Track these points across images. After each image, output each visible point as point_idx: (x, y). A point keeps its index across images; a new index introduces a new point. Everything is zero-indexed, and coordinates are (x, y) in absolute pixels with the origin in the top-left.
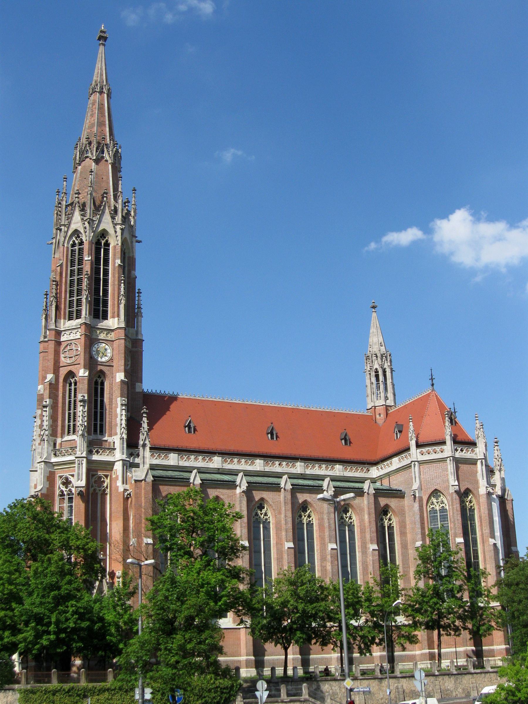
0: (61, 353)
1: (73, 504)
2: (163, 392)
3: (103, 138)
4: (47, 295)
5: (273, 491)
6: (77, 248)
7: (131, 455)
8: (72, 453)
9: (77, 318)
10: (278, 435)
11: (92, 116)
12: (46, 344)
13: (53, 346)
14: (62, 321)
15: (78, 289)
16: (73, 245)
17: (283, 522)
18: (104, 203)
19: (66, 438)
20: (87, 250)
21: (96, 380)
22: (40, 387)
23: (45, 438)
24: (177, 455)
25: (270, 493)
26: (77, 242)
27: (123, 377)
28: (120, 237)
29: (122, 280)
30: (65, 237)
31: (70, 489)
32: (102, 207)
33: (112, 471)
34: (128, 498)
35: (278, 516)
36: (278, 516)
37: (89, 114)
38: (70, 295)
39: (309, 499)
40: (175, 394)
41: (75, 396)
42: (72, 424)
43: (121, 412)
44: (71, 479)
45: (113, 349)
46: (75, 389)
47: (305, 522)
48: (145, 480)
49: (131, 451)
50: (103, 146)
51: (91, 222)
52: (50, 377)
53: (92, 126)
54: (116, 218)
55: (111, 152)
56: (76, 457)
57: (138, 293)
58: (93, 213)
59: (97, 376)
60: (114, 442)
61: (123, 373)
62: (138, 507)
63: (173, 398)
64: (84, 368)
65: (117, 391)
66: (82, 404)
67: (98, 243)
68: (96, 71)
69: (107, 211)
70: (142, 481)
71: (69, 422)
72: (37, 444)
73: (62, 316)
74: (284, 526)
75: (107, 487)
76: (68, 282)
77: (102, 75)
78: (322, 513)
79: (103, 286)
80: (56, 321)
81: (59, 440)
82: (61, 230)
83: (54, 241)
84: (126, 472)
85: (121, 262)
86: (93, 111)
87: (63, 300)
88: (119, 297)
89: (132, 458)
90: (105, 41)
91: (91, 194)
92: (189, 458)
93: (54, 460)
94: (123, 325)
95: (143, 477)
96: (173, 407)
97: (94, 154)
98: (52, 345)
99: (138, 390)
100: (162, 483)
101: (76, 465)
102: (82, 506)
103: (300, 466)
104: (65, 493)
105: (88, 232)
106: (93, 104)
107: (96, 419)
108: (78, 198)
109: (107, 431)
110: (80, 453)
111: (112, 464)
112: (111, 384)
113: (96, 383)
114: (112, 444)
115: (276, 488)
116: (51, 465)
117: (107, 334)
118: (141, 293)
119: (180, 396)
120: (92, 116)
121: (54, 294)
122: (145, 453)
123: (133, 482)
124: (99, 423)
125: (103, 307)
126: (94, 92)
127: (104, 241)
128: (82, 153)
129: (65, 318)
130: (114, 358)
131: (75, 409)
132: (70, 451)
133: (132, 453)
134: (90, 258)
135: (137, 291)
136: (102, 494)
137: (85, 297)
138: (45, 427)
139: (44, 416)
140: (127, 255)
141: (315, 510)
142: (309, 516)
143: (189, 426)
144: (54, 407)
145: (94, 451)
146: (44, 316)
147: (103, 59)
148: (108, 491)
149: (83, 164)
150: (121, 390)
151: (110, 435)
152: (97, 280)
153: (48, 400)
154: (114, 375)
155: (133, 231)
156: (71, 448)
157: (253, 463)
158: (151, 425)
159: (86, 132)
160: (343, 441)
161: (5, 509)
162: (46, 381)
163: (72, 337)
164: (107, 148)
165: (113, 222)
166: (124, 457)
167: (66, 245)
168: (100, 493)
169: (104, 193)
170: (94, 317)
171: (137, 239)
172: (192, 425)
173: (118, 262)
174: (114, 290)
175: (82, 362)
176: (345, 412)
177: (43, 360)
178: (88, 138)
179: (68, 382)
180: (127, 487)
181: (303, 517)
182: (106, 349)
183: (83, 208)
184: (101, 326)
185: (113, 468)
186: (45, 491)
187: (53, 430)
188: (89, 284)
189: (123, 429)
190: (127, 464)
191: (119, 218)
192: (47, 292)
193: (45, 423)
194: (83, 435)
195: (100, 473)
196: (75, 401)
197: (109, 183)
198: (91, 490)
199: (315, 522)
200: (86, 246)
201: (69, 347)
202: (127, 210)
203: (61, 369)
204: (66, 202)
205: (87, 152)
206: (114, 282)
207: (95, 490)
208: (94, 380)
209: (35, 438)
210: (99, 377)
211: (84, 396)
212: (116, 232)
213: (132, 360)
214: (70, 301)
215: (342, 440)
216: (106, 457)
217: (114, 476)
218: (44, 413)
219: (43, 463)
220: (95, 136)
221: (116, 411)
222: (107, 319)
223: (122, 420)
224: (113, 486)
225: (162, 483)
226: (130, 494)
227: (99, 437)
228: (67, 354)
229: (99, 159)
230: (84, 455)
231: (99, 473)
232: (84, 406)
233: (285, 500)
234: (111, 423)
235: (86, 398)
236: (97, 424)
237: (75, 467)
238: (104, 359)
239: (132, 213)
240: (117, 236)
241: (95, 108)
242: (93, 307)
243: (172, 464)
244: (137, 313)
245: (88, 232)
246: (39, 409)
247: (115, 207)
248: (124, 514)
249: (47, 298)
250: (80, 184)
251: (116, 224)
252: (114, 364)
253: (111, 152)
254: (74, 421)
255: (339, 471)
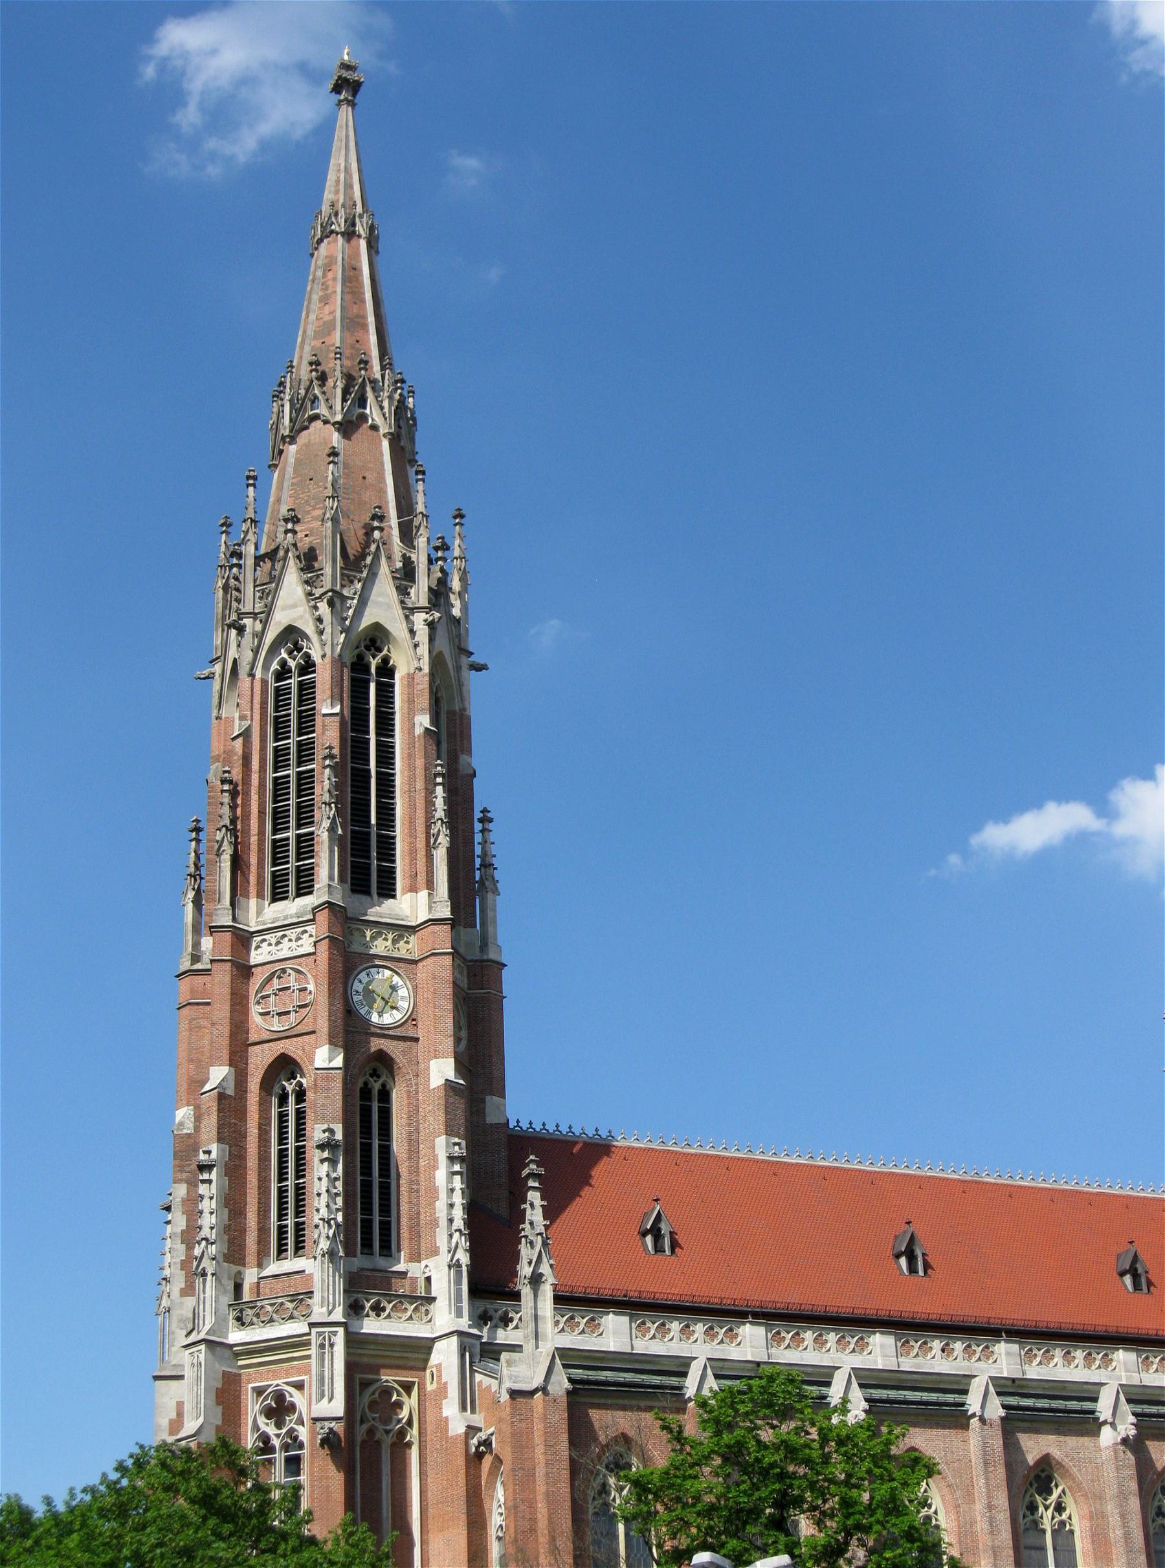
0: (252, 1000)
1: (303, 1478)
2: (564, 1129)
3: (361, 362)
4: (198, 830)
5: (944, 1427)
6: (293, 682)
7: (482, 1319)
8: (296, 1313)
9: (299, 895)
10: (928, 1259)
11: (325, 300)
12: (200, 980)
13: (227, 979)
14: (253, 902)
15: (299, 806)
16: (283, 673)
17: (982, 1526)
18: (373, 547)
19: (274, 1268)
20: (328, 686)
21: (366, 1084)
22: (183, 1114)
23: (209, 1266)
24: (626, 1319)
25: (934, 1432)
26: (292, 664)
27: (451, 1074)
28: (426, 646)
29: (436, 775)
30: (256, 651)
31: (292, 1430)
32: (369, 560)
33: (424, 1369)
34: (479, 1456)
35: (964, 1507)
36: (964, 1507)
37: (315, 297)
38: (275, 825)
39: (1056, 1454)
40: (604, 1133)
41: (300, 1134)
42: (290, 1222)
43: (450, 1180)
44: (296, 1398)
45: (415, 988)
46: (300, 1115)
47: (1047, 1525)
48: (544, 1389)
49: (483, 1305)
50: (363, 385)
51: (336, 600)
52: (219, 1074)
53: (328, 328)
54: (413, 591)
55: (386, 404)
56: (312, 1325)
57: (480, 820)
58: (342, 575)
59: (369, 1070)
60: (428, 1279)
61: (453, 1059)
62: (523, 1481)
63: (599, 1149)
64: (331, 1043)
65: (433, 1117)
66: (326, 1154)
67: (359, 667)
68: (331, 177)
69: (384, 569)
70: (532, 1393)
71: (281, 1215)
72: (176, 1292)
73: (253, 890)
74: (984, 1539)
75: (410, 1422)
76: (269, 785)
77: (349, 186)
78: (1100, 1497)
79: (377, 796)
80: (233, 904)
81: (250, 1276)
82: (241, 630)
83: (217, 668)
84: (472, 1372)
85: (432, 723)
86: (327, 289)
87: (254, 839)
88: (428, 827)
89: (486, 1329)
90: (355, 94)
91: (334, 520)
92: (663, 1330)
93: (236, 1336)
94: (445, 912)
95: (538, 1381)
96: (599, 1172)
97: (338, 407)
98: (223, 976)
99: (492, 1118)
100: (596, 1401)
101: (313, 1351)
102: (336, 1479)
103: (1008, 1354)
104: (276, 1442)
105: (328, 630)
106: (328, 267)
107: (367, 1208)
108: (294, 532)
109: (405, 1243)
110: (325, 1309)
111: (424, 1347)
112: (413, 1096)
113: (366, 1093)
114: (421, 1283)
115: (956, 1418)
116: (227, 1353)
117: (395, 941)
118: (491, 820)
119: (620, 1143)
120: (325, 300)
121: (227, 822)
122: (540, 1305)
123: (505, 1397)
124: (376, 1219)
125: (378, 859)
126: (327, 233)
127: (378, 659)
128: (298, 406)
129: (260, 895)
130: (421, 1015)
131: (298, 1176)
132: (290, 1306)
133: (485, 1312)
134: (337, 710)
135: (478, 815)
136: (393, 1445)
137: (326, 824)
138: (206, 1232)
139: (202, 1197)
140: (444, 707)
141: (1077, 1488)
142: (1060, 1508)
143: (656, 1232)
144: (234, 1169)
145: (368, 1305)
146: (191, 895)
147: (352, 144)
148: (413, 1434)
149: (303, 437)
150: (447, 1113)
151: (415, 1257)
152: (361, 778)
153: (214, 1147)
154: (422, 1066)
155: (459, 636)
156: (293, 1297)
157: (861, 1345)
158: (550, 1214)
159: (307, 349)
160: (1128, 1279)
161: (104, 1475)
162: (207, 1087)
163: (285, 950)
164: (373, 389)
165: (402, 602)
166: (464, 1323)
167: (258, 674)
168: (388, 1441)
169: (374, 517)
170: (353, 891)
171: (472, 659)
172: (665, 1228)
173: (423, 721)
174: (412, 808)
175: (323, 1025)
176: (1121, 1192)
177: (190, 1029)
178: (318, 363)
179: (277, 1090)
180: (478, 1419)
181: (1041, 1509)
182: (394, 988)
183: (309, 560)
184: (377, 915)
185: (427, 1360)
186: (209, 1437)
187: (231, 1242)
188: (337, 786)
189: (457, 1235)
190: (472, 1346)
191: (420, 593)
192: (198, 821)
193: (208, 1221)
194: (331, 1254)
195: (388, 1377)
196: (300, 1152)
197: (382, 492)
198: (361, 1431)
199: (1079, 1526)
200: (323, 677)
201: (275, 980)
202: (442, 570)
203: (252, 1049)
204: (257, 548)
205: (313, 402)
206: (411, 781)
207: (371, 1432)
208: (360, 1084)
209: (167, 1272)
210: (375, 1074)
211: (332, 1131)
212: (412, 632)
213: (469, 1027)
214: (275, 841)
215: (1122, 1274)
216: (406, 1325)
217: (430, 1387)
218: (203, 1189)
219: (203, 1347)
220: (339, 354)
221: (432, 1178)
222: (394, 897)
223: (451, 1206)
224: (430, 1417)
225: (596, 1401)
226: (487, 1443)
227: (381, 1262)
228: (272, 1004)
229: (351, 422)
230: (338, 1315)
231: (384, 1378)
232: (333, 1162)
233: (985, 1454)
234: (415, 1216)
235: (339, 1136)
236: (370, 1222)
237: (309, 1357)
238: (389, 1018)
239: (456, 584)
240: (416, 646)
241: (335, 279)
242: (349, 859)
243: (612, 1349)
244: (482, 882)
245: (328, 630)
246: (181, 1181)
247: (407, 561)
248: (468, 1507)
249: (198, 841)
250: (295, 497)
251: (413, 610)
252: (420, 1034)
253: (386, 404)
254: (299, 1212)
255: (1127, 1371)
